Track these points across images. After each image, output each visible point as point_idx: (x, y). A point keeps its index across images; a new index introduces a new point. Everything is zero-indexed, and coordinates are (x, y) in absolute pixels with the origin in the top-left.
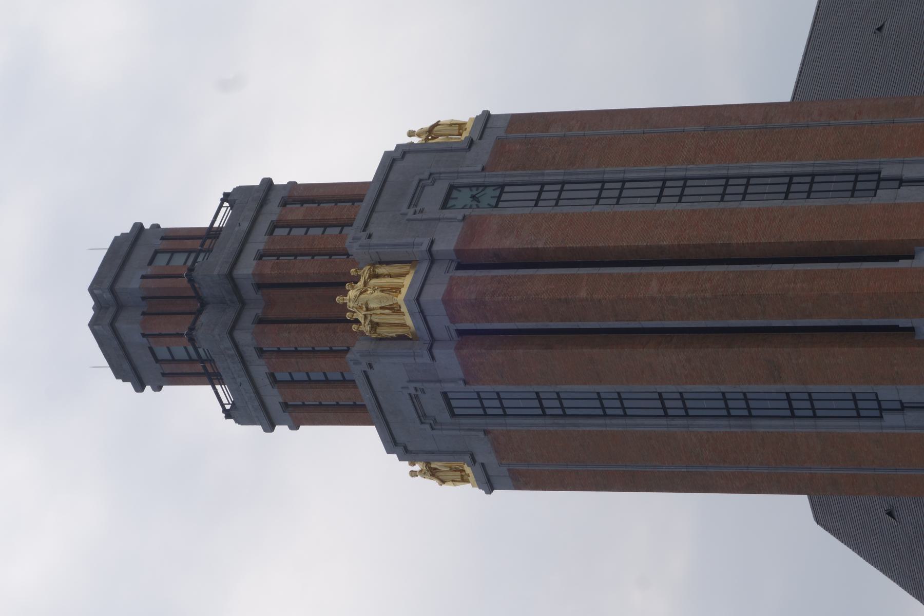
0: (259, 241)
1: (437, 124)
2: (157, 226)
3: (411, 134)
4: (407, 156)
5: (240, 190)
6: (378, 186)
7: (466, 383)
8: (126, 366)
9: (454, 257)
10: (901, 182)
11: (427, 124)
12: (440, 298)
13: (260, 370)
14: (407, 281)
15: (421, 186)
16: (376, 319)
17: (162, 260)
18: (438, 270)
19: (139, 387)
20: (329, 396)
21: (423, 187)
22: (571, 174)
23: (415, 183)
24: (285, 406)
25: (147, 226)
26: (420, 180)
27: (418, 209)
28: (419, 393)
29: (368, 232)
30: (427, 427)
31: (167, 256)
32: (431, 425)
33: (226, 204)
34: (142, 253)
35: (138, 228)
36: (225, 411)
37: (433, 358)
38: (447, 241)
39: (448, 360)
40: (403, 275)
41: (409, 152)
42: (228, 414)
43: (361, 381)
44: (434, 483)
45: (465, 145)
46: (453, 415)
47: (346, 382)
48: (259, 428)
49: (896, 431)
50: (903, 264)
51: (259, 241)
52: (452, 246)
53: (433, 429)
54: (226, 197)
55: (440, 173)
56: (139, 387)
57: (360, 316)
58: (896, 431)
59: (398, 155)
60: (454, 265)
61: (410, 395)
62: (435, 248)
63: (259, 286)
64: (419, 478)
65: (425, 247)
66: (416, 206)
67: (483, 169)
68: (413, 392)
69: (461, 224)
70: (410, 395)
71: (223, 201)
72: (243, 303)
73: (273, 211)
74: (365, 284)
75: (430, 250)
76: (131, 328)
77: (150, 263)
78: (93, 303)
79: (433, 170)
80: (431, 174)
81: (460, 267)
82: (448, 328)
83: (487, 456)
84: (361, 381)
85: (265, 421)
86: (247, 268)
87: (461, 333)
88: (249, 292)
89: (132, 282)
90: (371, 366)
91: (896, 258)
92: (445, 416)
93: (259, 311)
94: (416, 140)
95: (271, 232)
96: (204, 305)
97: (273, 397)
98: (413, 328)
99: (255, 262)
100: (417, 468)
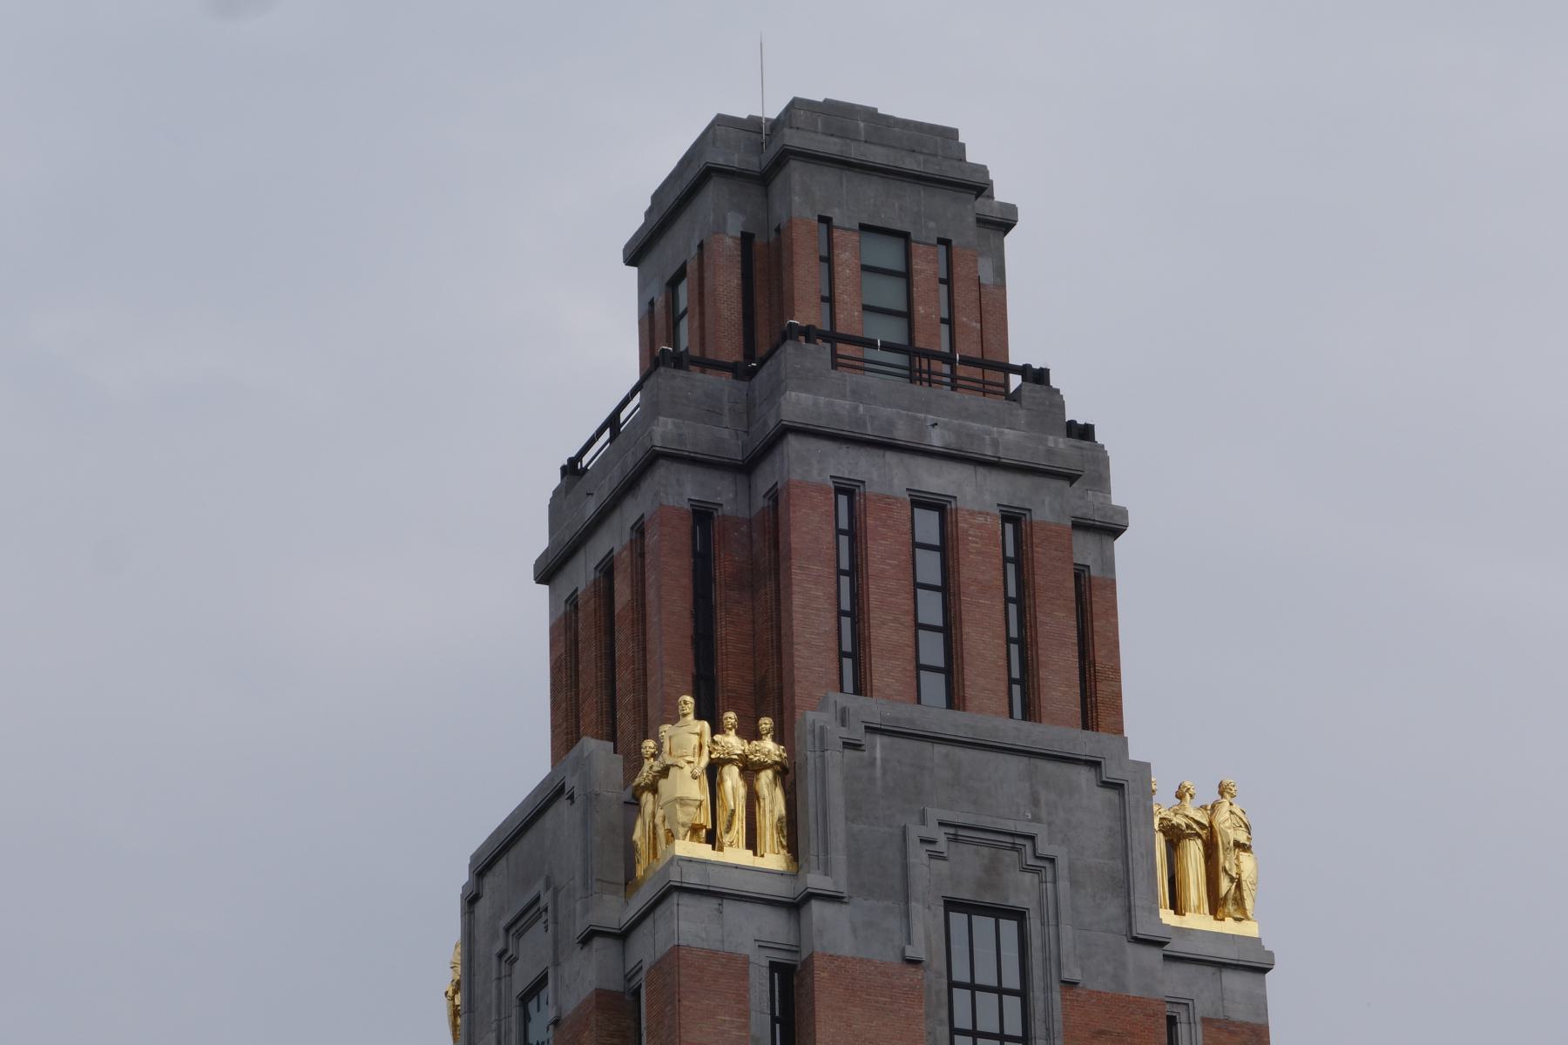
4: (1112, 795)
8: (670, 201)
9: (804, 955)
14: (736, 854)
18: (773, 925)
21: (1014, 848)
23: (1023, 828)
26: (1032, 838)
27: (942, 845)
28: (544, 918)
29: (866, 739)
30: (499, 946)
32: (505, 951)
38: (833, 931)
39: (586, 974)
40: (752, 843)
41: (1122, 795)
45: (1142, 930)
53: (500, 956)
55: (1055, 882)
59: (1111, 772)
61: (538, 899)
63: (774, 496)
66: (955, 839)
67: (1070, 985)
68: (542, 904)
69: (892, 956)
70: (538, 899)
75: (810, 896)
79: (1062, 864)
80: (1052, 860)
92: (520, 984)
93: (727, 509)
95: (921, 501)
96: (743, 371)
97: (582, 574)
99: (687, 506)
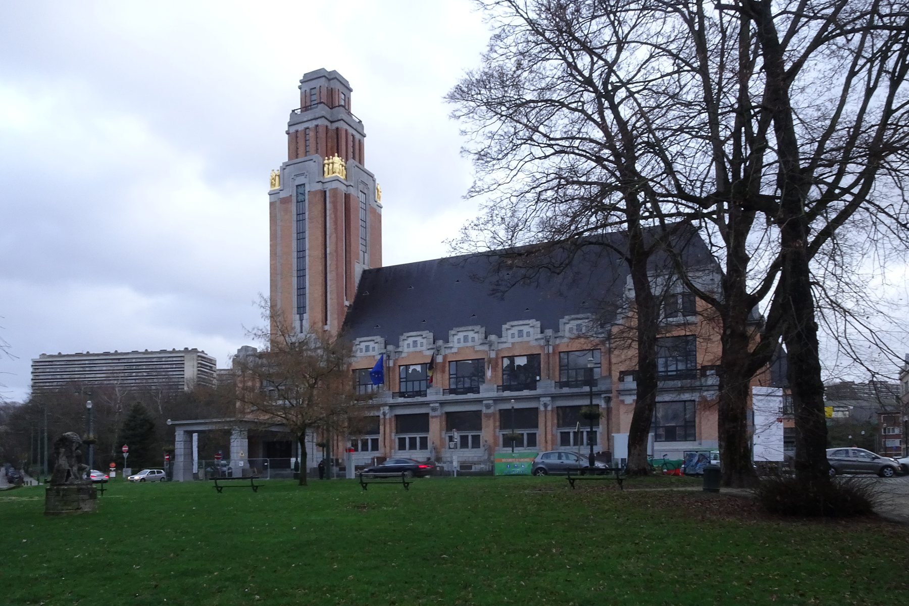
0: (351, 131)
13: (312, 125)
17: (343, 96)
18: (345, 187)
22: (42, 457)
34: (345, 91)
35: (351, 90)
43: (306, 158)
46: (297, 186)
47: (306, 153)
49: (203, 421)
51: (351, 131)
54: (360, 122)
56: (302, 82)
57: (331, 161)
58: (203, 421)
63: (337, 129)
72: (332, 122)
73: (357, 136)
83: (283, 195)
84: (306, 158)
86: (341, 125)
87: (325, 192)
89: (335, 85)
92: (297, 183)
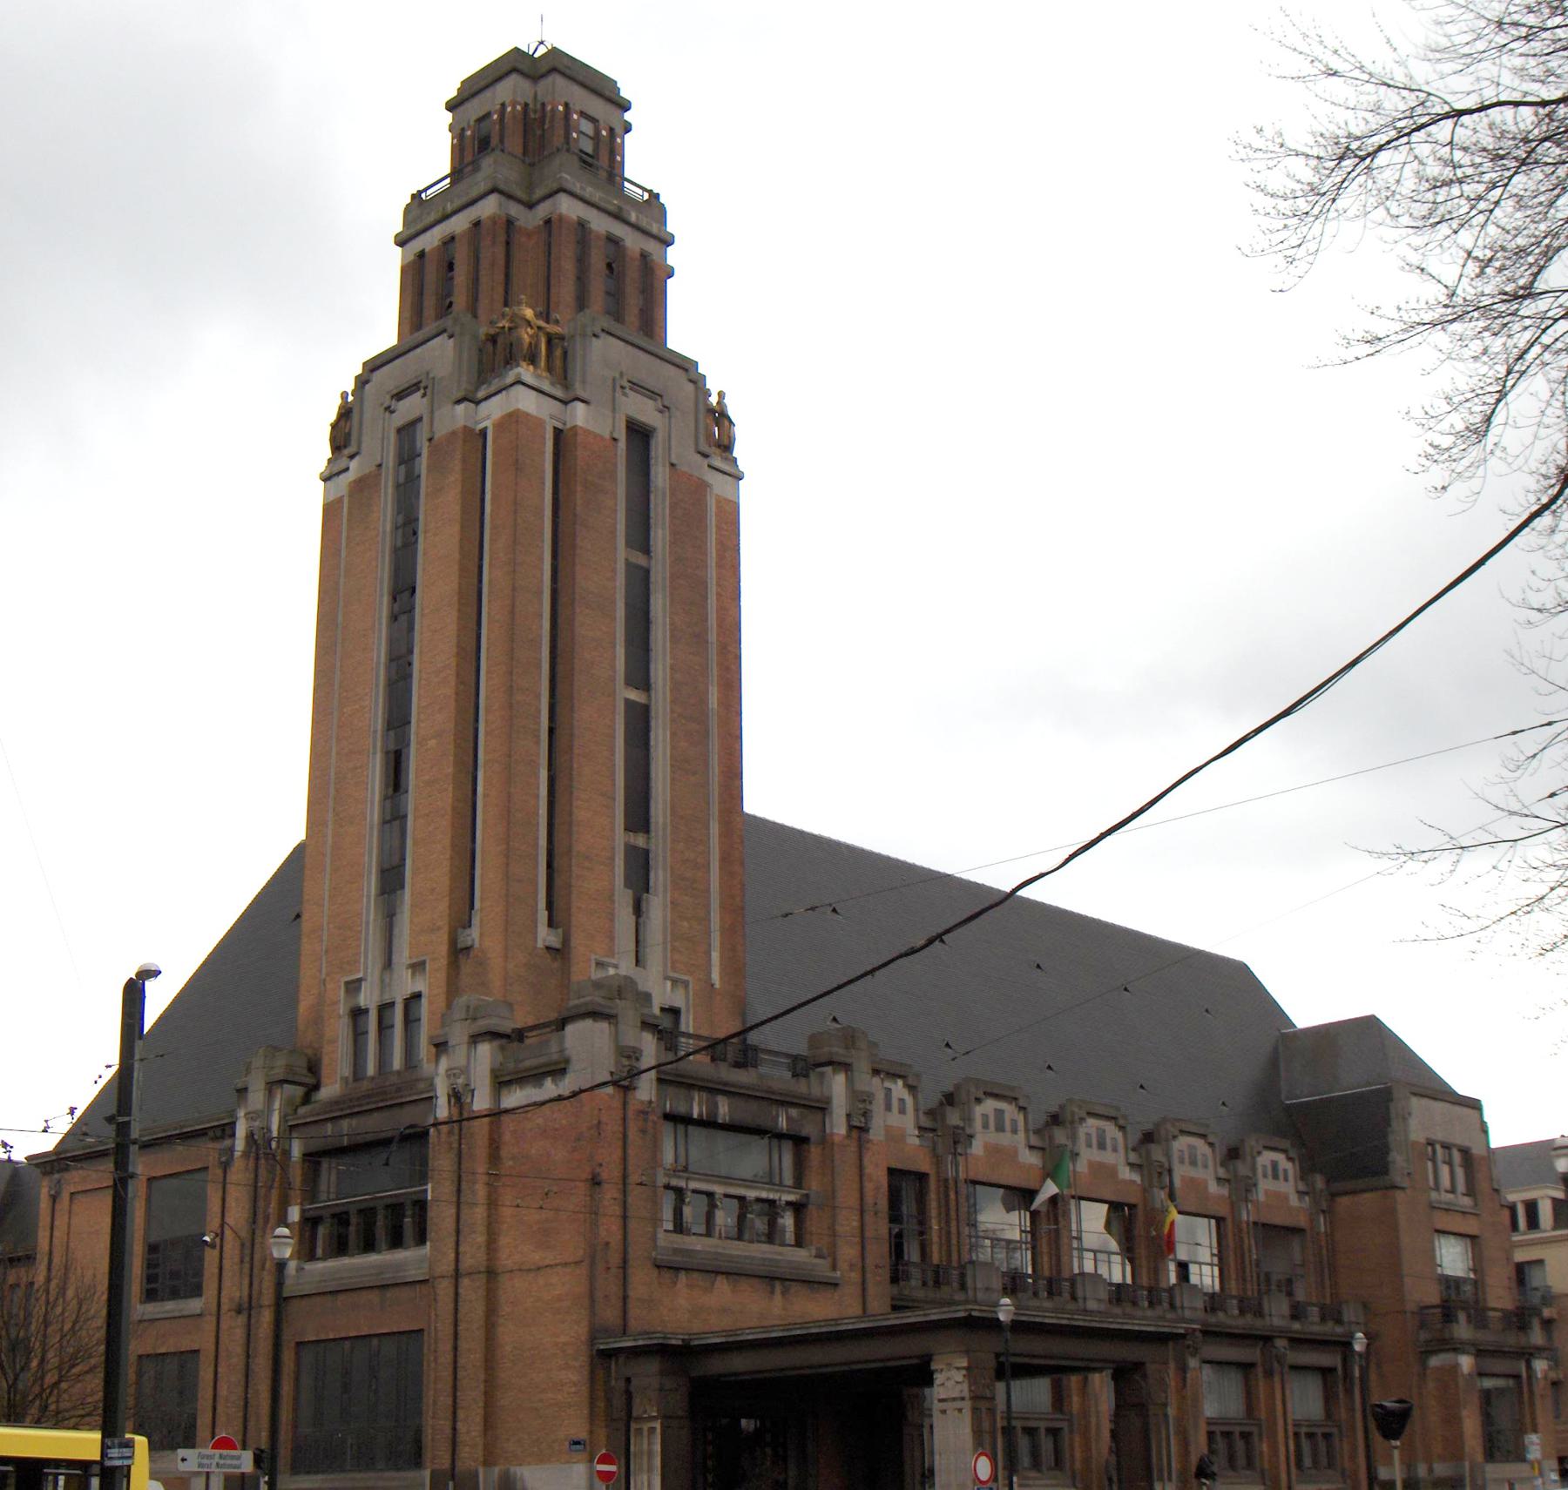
1: (731, 422)
2: (628, 128)
3: (721, 395)
4: (691, 387)
5: (662, 210)
6: (661, 353)
7: (430, 440)
10: (638, 909)
11: (732, 412)
12: (520, 406)
15: (653, 394)
16: (500, 340)
17: (586, 127)
19: (452, 106)
20: (430, 303)
24: (421, 255)
25: (628, 116)
31: (591, 133)
33: (646, 196)
34: (597, 107)
36: (420, 192)
37: (459, 402)
42: (416, 197)
44: (333, 417)
48: (400, 228)
50: (543, 915)
52: (580, 422)
54: (655, 197)
59: (693, 376)
60: (560, 426)
62: (580, 406)
63: (548, 222)
64: (339, 401)
65: (580, 393)
67: (672, 465)
69: (607, 435)
71: (650, 192)
72: (530, 206)
73: (633, 242)
74: (539, 328)
76: (509, 91)
77: (582, 114)
78: (622, 94)
81: (558, 433)
82: (488, 417)
85: (405, 236)
87: (483, 433)
88: (543, 210)
89: (561, 91)
90: (451, 337)
91: (550, 906)
94: (714, 400)
98: (1193, 1363)
100: (350, 398)
